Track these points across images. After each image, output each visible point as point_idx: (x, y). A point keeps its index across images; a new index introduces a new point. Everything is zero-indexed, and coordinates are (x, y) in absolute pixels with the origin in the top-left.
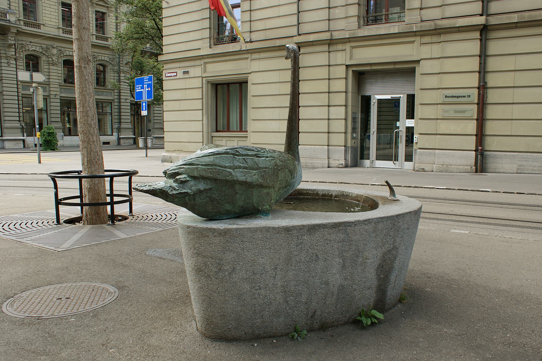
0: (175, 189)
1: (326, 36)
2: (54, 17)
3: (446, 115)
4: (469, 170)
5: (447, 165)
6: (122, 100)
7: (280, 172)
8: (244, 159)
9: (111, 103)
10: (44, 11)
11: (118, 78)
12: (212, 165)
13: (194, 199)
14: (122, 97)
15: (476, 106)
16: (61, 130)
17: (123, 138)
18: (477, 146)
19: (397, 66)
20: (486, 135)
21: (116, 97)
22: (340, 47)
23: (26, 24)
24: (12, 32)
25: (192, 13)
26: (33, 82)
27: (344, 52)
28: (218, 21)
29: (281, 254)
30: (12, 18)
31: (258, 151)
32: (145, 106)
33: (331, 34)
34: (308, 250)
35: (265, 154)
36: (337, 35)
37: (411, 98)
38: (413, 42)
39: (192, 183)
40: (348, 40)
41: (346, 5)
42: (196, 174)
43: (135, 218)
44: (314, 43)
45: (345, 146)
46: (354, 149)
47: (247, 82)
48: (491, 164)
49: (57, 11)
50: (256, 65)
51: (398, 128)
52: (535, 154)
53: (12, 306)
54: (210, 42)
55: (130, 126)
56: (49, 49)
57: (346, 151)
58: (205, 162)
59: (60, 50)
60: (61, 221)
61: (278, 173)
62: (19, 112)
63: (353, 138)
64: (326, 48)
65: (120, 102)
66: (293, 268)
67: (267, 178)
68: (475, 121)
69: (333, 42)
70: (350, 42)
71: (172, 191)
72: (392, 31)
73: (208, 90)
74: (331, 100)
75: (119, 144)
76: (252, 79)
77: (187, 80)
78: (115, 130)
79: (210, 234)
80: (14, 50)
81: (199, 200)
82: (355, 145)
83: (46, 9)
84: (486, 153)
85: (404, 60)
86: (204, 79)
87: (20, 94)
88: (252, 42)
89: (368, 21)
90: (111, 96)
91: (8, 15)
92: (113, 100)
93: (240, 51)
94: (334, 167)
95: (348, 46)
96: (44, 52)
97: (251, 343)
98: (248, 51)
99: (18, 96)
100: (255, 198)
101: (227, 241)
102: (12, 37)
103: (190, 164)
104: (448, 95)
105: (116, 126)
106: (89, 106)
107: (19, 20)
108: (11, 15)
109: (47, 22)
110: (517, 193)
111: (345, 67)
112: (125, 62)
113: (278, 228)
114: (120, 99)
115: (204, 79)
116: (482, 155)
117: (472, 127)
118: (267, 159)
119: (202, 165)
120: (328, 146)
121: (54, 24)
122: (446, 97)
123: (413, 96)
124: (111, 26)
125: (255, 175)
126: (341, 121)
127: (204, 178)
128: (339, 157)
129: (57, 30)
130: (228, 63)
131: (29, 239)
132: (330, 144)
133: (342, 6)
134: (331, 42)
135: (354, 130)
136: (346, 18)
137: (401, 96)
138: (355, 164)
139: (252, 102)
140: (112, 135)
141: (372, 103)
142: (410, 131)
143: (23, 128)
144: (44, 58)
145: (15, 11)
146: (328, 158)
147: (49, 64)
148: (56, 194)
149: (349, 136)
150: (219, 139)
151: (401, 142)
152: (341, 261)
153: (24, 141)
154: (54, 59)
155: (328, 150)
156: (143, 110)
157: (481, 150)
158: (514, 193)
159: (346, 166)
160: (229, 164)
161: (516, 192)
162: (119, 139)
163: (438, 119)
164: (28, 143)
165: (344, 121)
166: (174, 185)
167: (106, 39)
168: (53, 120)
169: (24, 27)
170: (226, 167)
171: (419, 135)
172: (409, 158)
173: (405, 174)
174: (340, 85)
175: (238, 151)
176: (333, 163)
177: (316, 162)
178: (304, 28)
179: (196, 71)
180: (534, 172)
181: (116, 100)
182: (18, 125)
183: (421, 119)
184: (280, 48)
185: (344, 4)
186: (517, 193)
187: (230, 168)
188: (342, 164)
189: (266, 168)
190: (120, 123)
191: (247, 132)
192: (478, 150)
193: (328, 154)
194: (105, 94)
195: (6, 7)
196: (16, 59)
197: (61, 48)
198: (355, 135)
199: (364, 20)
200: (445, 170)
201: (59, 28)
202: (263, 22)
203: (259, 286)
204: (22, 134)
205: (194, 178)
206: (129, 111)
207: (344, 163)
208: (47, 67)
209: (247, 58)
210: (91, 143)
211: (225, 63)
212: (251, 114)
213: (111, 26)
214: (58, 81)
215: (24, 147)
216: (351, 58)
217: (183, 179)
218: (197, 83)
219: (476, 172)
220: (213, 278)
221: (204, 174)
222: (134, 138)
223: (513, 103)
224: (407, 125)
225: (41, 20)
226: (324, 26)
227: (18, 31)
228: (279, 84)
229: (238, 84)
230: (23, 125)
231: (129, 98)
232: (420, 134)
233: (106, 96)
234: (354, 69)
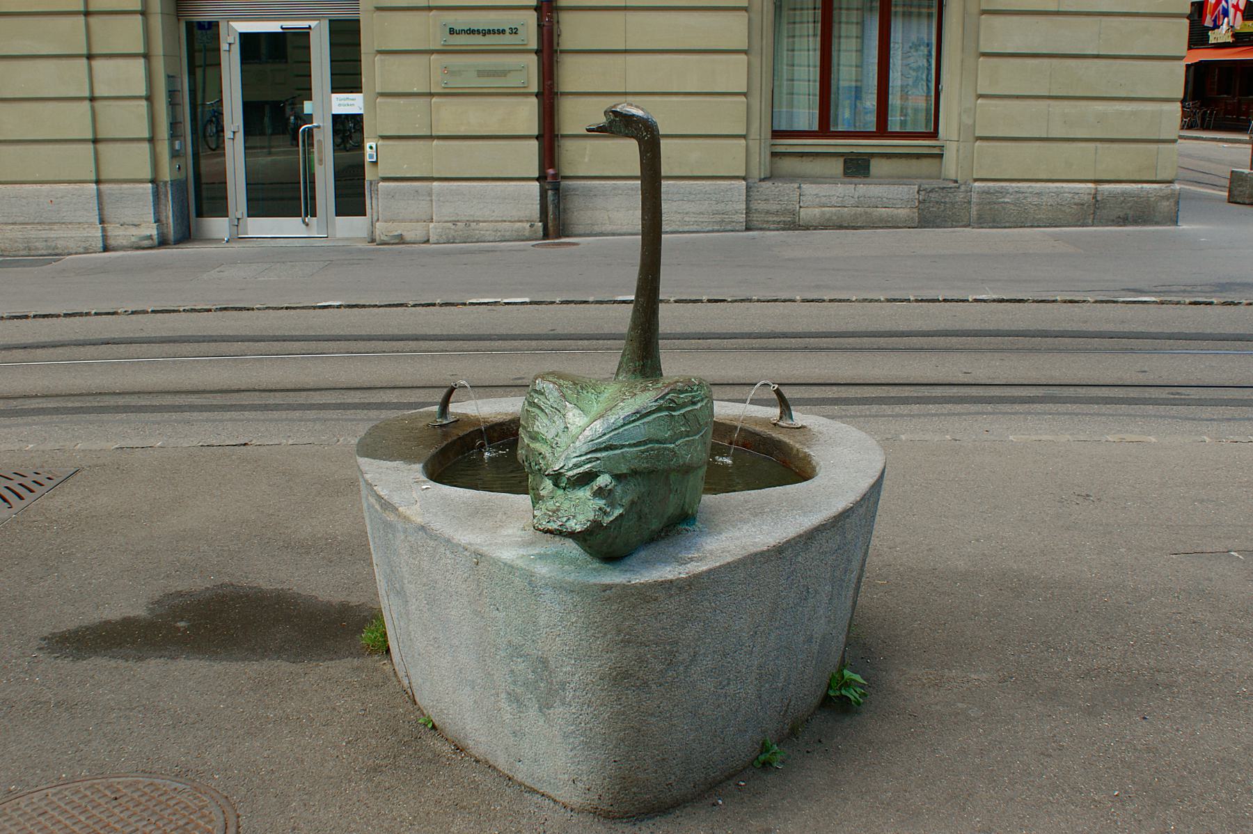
3: (457, 83)
4: (527, 234)
5: (468, 223)
15: (534, 58)
18: (542, 168)
20: (563, 136)
42: (624, 469)
45: (153, 181)
46: (179, 186)
48: (581, 214)
51: (309, 119)
52: (692, 182)
63: (175, 154)
68: (535, 100)
74: (95, 38)
82: (182, 176)
84: (564, 183)
94: (124, 248)
97: (711, 801)
103: (606, 449)
104: (457, 28)
110: (709, 301)
116: (557, 189)
117: (524, 115)
119: (630, 446)
120: (98, 182)
122: (452, 31)
126: (87, 87)
128: (138, 217)
132: (103, 177)
137: (313, 24)
138: (186, 235)
141: (224, 46)
142: (348, 130)
146: (102, 221)
149: (164, 149)
151: (321, 161)
155: (99, 194)
157: (555, 176)
158: (701, 301)
159: (163, 242)
161: (705, 298)
163: (431, 95)
165: (144, 103)
171: (380, 142)
173: (344, 255)
176: (118, 234)
177: (64, 236)
180: (686, 228)
183: (382, 95)
186: (709, 301)
188: (150, 237)
192: (546, 178)
193: (101, 209)
200: (463, 238)
207: (155, 232)
219: (546, 235)
220: (654, 686)
221: (635, 464)
223: (626, 51)
224: (337, 110)
232: (383, 138)
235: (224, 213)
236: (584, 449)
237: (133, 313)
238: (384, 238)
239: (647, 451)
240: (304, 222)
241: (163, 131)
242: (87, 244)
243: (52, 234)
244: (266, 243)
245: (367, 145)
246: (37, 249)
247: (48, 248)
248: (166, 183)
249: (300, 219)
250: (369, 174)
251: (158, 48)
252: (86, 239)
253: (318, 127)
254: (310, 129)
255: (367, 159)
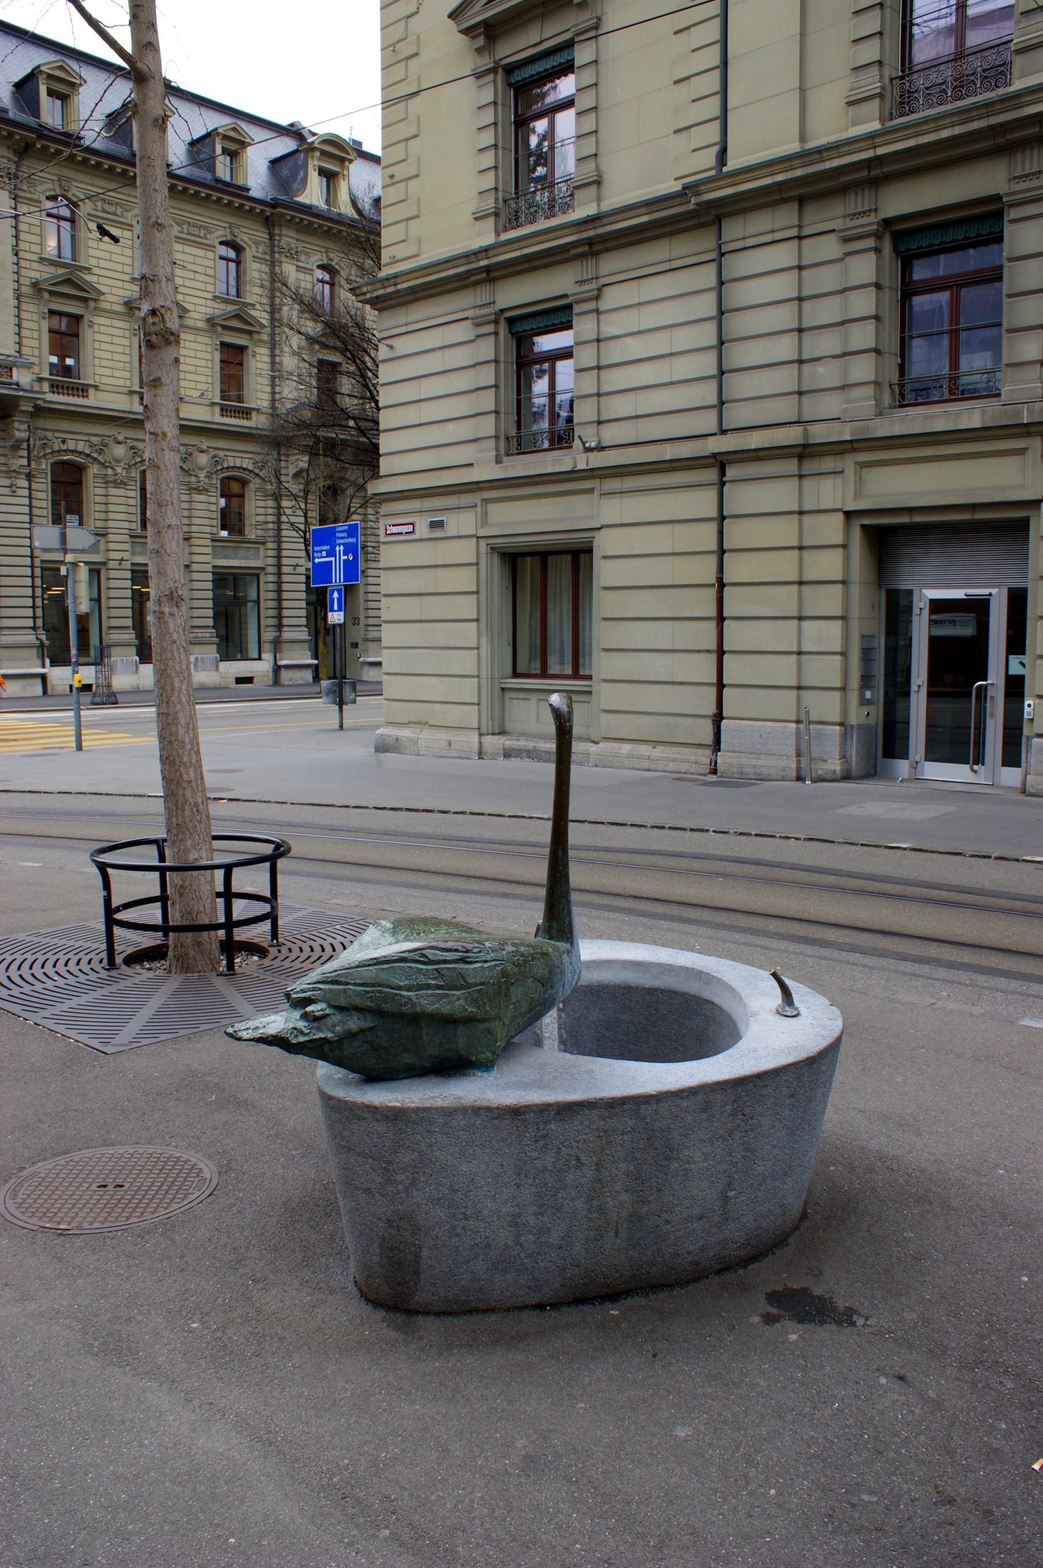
0: (302, 1033)
1: (790, 436)
2: (120, 349)
6: (285, 569)
7: (513, 989)
8: (437, 970)
9: (258, 576)
10: (98, 354)
11: (276, 526)
12: (373, 985)
13: (341, 1049)
14: (285, 561)
16: (133, 650)
17: (288, 667)
19: (980, 516)
21: (271, 561)
22: (828, 464)
23: (55, 387)
24: (23, 412)
25: (452, 375)
26: (65, 551)
27: (839, 480)
28: (519, 393)
29: (505, 1156)
30: (22, 377)
31: (467, 951)
32: (339, 599)
33: (806, 430)
34: (558, 1148)
35: (483, 956)
36: (820, 434)
37: (1018, 601)
38: (1022, 452)
39: (337, 1017)
40: (849, 446)
41: (845, 354)
42: (343, 1002)
43: (284, 950)
44: (760, 454)
47: (590, 551)
49: (127, 350)
50: (612, 510)
53: (15, 1196)
54: (497, 449)
55: (304, 635)
56: (106, 445)
57: (845, 737)
58: (361, 979)
59: (132, 448)
60: (119, 959)
61: (508, 990)
62: (34, 607)
63: (863, 702)
64: (791, 466)
65: (279, 574)
66: (530, 1181)
67: (485, 1004)
69: (809, 450)
70: (854, 450)
71: (296, 1036)
72: (964, 424)
73: (494, 571)
75: (276, 681)
76: (605, 543)
77: (440, 544)
78: (267, 647)
79: (368, 1115)
80: (25, 453)
81: (348, 1049)
82: (872, 720)
83: (104, 346)
85: (997, 499)
86: (483, 543)
87: (37, 562)
88: (603, 449)
89: (902, 396)
90: (257, 558)
91: (15, 371)
92: (263, 569)
93: (572, 472)
95: (848, 463)
96: (95, 455)
98: (592, 473)
99: (32, 567)
100: (461, 1041)
101: (400, 1129)
102: (22, 422)
103: (332, 982)
105: (268, 635)
106: (180, 702)
107: (40, 380)
108: (23, 371)
109: (104, 380)
111: (840, 517)
112: (292, 470)
113: (497, 1108)
114: (279, 565)
115: (483, 543)
118: (486, 965)
119: (355, 984)
121: (121, 382)
123: (1024, 591)
124: (259, 395)
125: (459, 999)
127: (358, 1009)
129: (127, 397)
130: (543, 501)
131: (47, 1013)
133: (834, 357)
134: (804, 452)
135: (866, 680)
136: (843, 387)
137: (994, 591)
138: (871, 772)
139: (603, 603)
140: (260, 659)
143: (42, 645)
144: (94, 470)
145: (33, 360)
147: (107, 483)
148: (108, 901)
149: (854, 698)
150: (521, 695)
151: (992, 716)
152: (631, 1168)
153: (43, 678)
154: (119, 470)
156: (332, 610)
159: (846, 777)
160: (407, 982)
162: (277, 669)
164: (55, 682)
166: (301, 1024)
167: (246, 413)
168: (114, 623)
169: (50, 397)
170: (400, 988)
171: (1037, 701)
172: (1012, 756)
174: (827, 565)
175: (424, 956)
178: (737, 416)
179: (461, 523)
181: (270, 570)
182: (30, 638)
184: (675, 465)
185: (838, 352)
187: (409, 989)
189: (482, 984)
190: (280, 627)
191: (589, 678)
194: (242, 553)
195: (11, 350)
196: (29, 477)
197: (135, 443)
198: (868, 695)
199: (892, 391)
201: (132, 393)
202: (630, 397)
203: (464, 1214)
204: (39, 662)
205: (340, 1009)
206: (303, 595)
207: (838, 768)
208: (101, 491)
209: (591, 491)
210: (185, 785)
211: (534, 502)
212: (602, 634)
213: (259, 380)
214: (126, 525)
215: (45, 692)
216: (858, 494)
217: (317, 1014)
218: (465, 551)
220: (377, 1195)
222: (317, 666)
225: (91, 374)
226: (785, 409)
227: (37, 407)
228: (670, 558)
229: (569, 557)
230: (44, 638)
231: (302, 562)
233: (246, 558)
234: (867, 521)
235: (905, 756)
236: (315, 980)
237: (741, 834)
238: (1032, 790)
239: (373, 992)
240: (972, 769)
241: (855, 682)
242: (784, 773)
243: (759, 763)
244: (939, 786)
245: (1026, 703)
246: (747, 773)
247: (756, 773)
248: (852, 726)
249: (967, 767)
250: (1026, 732)
251: (855, 611)
252: (784, 769)
253: (992, 684)
254: (986, 686)
255: (1026, 716)
